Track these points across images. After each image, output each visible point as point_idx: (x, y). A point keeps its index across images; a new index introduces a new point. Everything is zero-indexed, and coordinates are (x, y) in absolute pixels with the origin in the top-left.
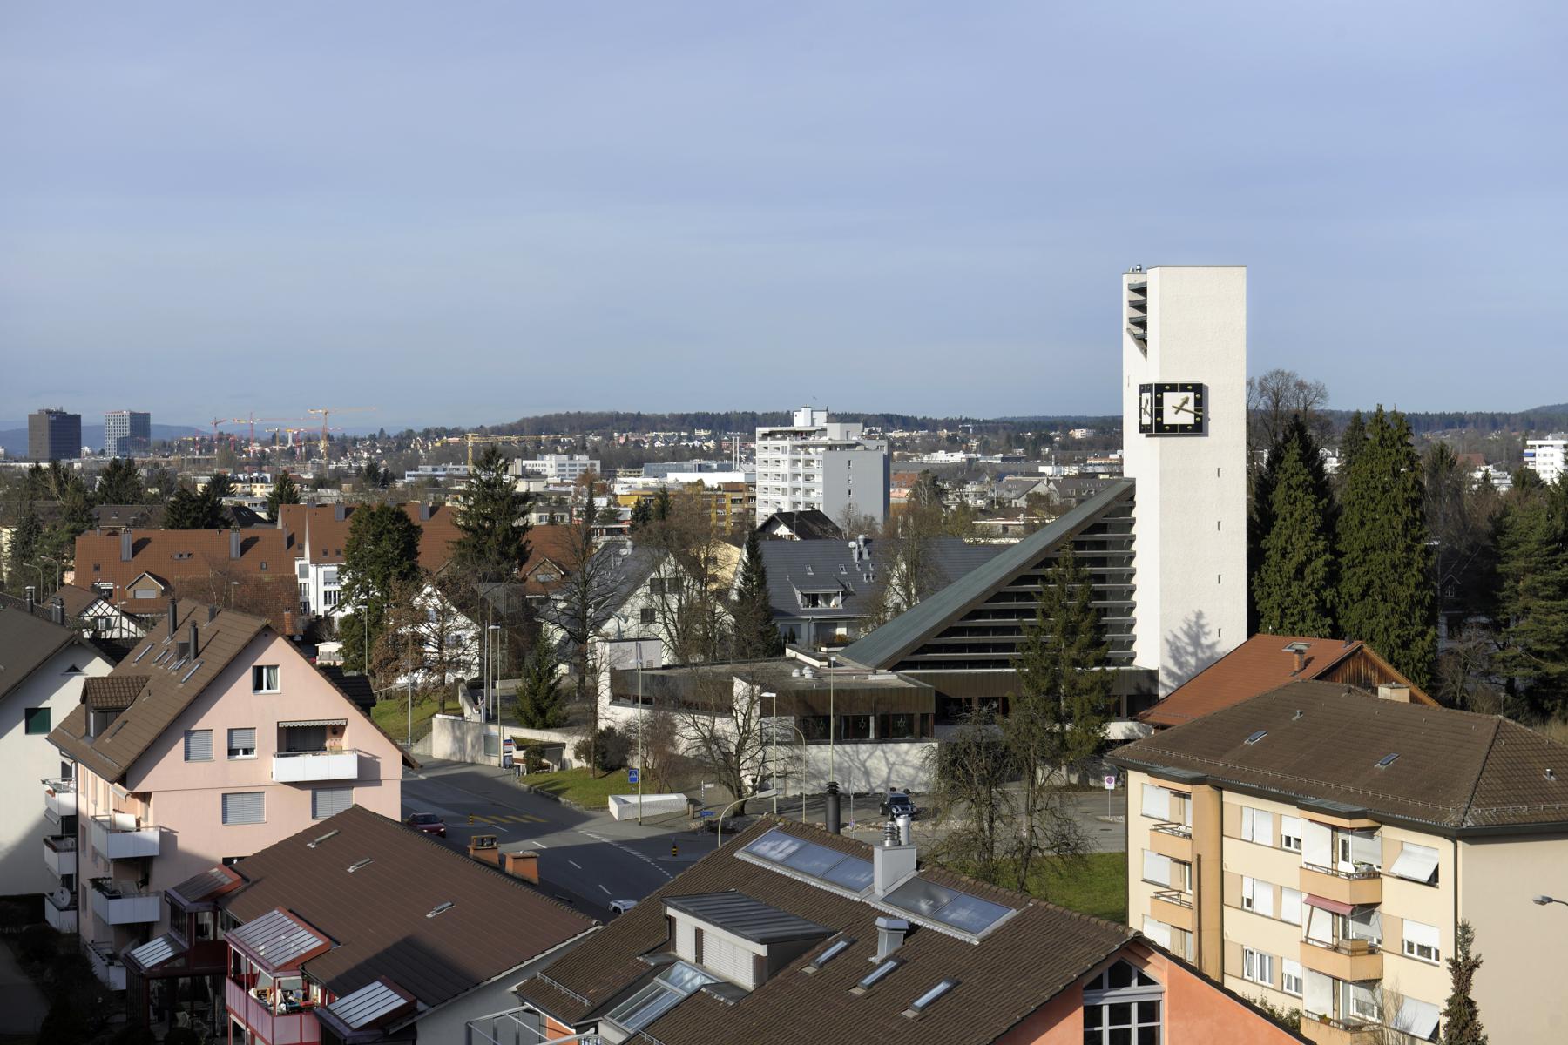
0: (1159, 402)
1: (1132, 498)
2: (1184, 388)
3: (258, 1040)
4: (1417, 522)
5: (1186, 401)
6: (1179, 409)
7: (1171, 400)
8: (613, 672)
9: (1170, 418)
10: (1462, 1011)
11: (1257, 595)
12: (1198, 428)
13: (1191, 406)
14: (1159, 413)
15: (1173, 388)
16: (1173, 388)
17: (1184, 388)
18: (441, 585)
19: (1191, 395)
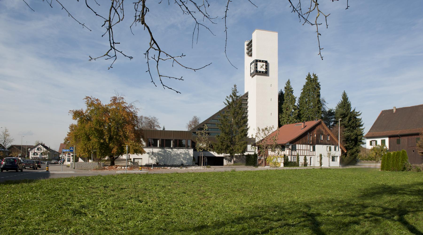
0: (256, 65)
1: (247, 96)
2: (263, 61)
3: (315, 1)
4: (199, 140)
5: (263, 65)
6: (261, 67)
7: (259, 64)
8: (96, 151)
9: (259, 69)
10: (419, 193)
11: (281, 120)
12: (266, 73)
13: (264, 67)
14: (256, 68)
15: (260, 61)
16: (260, 61)
17: (263, 61)
18: (255, 155)
19: (264, 64)
